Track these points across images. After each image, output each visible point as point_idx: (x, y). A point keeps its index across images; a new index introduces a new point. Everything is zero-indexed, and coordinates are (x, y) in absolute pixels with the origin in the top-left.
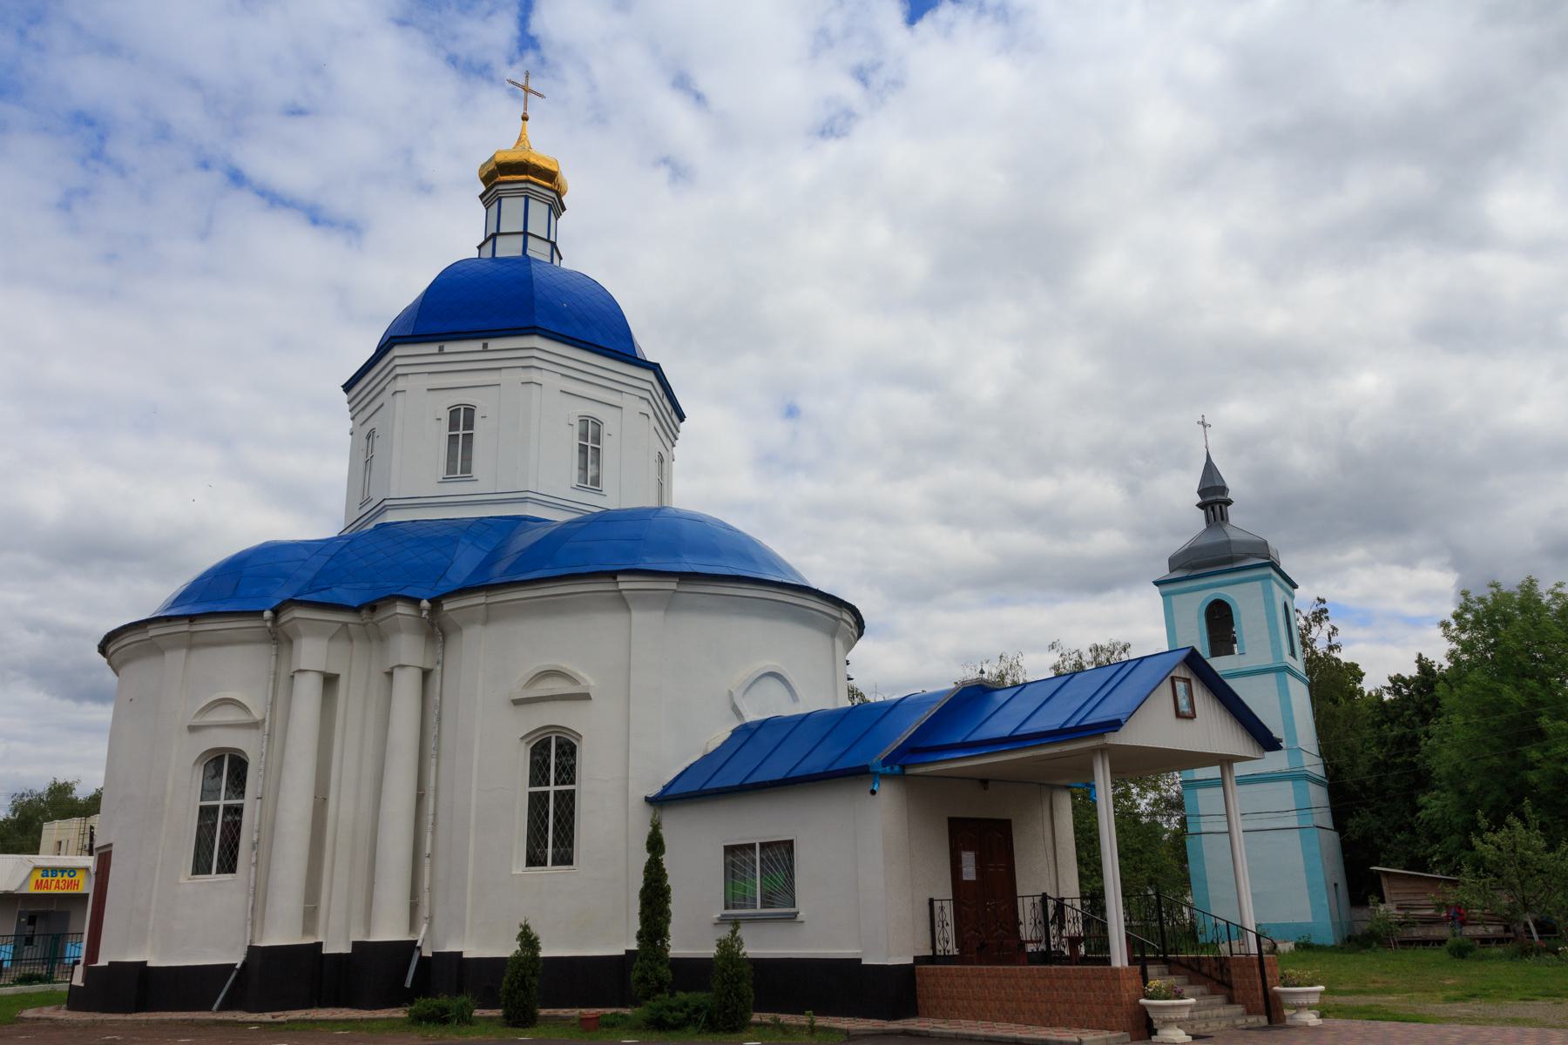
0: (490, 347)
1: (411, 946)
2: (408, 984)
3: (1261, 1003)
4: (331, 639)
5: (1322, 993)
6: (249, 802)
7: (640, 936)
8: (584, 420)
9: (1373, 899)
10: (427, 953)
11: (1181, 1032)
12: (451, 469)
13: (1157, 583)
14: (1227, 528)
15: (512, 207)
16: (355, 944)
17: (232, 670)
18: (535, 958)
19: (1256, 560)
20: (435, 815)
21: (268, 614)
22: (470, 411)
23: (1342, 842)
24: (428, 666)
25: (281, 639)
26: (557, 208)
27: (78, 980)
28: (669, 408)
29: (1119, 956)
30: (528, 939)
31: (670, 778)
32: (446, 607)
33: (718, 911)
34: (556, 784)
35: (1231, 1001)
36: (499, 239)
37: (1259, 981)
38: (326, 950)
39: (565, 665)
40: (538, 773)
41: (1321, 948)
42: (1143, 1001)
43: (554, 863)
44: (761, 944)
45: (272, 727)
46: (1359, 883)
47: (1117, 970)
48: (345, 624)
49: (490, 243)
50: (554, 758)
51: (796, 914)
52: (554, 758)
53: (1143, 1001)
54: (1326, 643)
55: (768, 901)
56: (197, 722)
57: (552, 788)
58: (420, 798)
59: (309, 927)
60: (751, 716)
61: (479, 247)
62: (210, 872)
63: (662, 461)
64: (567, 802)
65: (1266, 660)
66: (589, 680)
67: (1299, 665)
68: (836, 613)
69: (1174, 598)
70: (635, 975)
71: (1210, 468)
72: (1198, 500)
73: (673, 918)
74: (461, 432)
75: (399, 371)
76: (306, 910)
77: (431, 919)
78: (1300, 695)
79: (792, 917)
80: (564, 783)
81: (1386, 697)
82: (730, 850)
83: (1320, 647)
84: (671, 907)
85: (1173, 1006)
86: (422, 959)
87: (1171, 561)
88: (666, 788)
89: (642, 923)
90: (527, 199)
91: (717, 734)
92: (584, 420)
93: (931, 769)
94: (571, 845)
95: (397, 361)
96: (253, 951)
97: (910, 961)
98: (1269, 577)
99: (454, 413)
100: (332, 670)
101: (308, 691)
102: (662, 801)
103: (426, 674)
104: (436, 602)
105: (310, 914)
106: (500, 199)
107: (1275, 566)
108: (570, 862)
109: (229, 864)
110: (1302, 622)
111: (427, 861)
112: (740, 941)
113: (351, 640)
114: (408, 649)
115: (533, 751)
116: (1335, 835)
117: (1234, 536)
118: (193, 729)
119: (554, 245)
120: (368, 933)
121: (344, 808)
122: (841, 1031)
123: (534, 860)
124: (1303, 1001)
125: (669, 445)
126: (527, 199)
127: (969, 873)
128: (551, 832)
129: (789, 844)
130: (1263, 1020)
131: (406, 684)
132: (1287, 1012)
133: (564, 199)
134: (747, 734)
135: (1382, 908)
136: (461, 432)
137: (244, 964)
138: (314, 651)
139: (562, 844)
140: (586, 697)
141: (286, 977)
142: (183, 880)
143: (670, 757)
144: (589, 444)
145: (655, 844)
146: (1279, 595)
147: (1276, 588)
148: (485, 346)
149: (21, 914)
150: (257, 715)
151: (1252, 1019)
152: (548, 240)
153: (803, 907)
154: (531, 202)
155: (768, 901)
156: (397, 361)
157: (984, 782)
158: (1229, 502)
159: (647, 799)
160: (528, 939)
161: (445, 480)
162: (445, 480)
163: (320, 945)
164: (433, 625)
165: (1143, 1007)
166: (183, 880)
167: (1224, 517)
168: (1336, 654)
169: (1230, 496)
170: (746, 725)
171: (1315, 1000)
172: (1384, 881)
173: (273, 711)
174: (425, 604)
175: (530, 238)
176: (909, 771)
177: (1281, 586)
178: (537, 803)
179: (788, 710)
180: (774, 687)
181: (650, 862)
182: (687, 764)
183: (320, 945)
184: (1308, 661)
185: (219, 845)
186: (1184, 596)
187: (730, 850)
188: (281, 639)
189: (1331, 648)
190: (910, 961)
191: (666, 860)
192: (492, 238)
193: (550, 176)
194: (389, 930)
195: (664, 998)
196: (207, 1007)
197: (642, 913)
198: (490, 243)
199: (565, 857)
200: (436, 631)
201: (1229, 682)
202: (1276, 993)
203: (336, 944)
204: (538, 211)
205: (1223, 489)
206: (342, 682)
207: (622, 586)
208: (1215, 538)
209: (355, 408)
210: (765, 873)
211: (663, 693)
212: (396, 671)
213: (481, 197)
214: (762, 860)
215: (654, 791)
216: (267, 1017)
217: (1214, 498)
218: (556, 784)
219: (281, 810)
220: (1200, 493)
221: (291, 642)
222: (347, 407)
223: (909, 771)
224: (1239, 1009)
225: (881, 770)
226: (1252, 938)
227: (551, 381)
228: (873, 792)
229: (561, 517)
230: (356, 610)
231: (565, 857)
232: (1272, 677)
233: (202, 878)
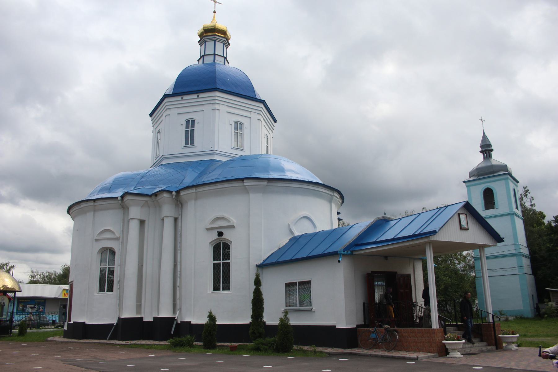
0: (184, 98)
1: (173, 319)
2: (172, 333)
3: (494, 341)
4: (142, 207)
7: (252, 317)
8: (236, 123)
9: (546, 300)
10: (179, 322)
11: (459, 353)
12: (186, 143)
13: (464, 182)
14: (492, 160)
15: (210, 45)
16: (154, 318)
17: (109, 220)
18: (215, 324)
19: (502, 172)
20: (181, 271)
22: (193, 121)
23: (535, 279)
24: (176, 217)
26: (227, 44)
27: (65, 328)
28: (270, 117)
29: (435, 323)
30: (212, 318)
31: (266, 257)
33: (283, 308)
34: (223, 260)
35: (482, 341)
36: (205, 57)
37: (493, 333)
38: (145, 319)
39: (225, 215)
40: (216, 257)
41: (527, 319)
42: (444, 342)
43: (223, 289)
44: (295, 321)
45: (123, 239)
46: (541, 293)
47: (434, 329)
48: (147, 201)
49: (202, 59)
50: (222, 250)
51: (312, 309)
52: (222, 250)
53: (444, 342)
54: (530, 204)
55: (301, 304)
56: (98, 238)
57: (221, 262)
58: (175, 266)
59: (139, 312)
60: (297, 233)
61: (198, 61)
63: (267, 138)
64: (227, 267)
65: (507, 211)
66: (234, 221)
67: (519, 212)
68: (332, 194)
69: (471, 187)
70: (250, 331)
71: (485, 137)
72: (480, 150)
73: (265, 310)
74: (190, 129)
75: (217, 102)
76: (137, 305)
77: (180, 309)
78: (520, 224)
80: (226, 260)
81: (553, 225)
82: (288, 285)
83: (528, 205)
84: (264, 306)
85: (456, 343)
86: (177, 324)
87: (470, 173)
88: (264, 261)
89: (253, 312)
90: (215, 41)
91: (284, 240)
92: (236, 123)
93: (363, 252)
94: (229, 283)
96: (119, 319)
97: (355, 327)
98: (508, 178)
99: (187, 122)
100: (143, 218)
101: (134, 226)
102: (261, 267)
103: (176, 220)
104: (178, 192)
105: (139, 307)
106: (205, 42)
107: (510, 174)
108: (229, 289)
109: (110, 289)
110: (520, 196)
111: (178, 288)
112: (288, 319)
113: (149, 207)
116: (533, 277)
117: (494, 163)
118: (97, 240)
119: (225, 58)
120: (158, 314)
121: (148, 269)
122: (327, 353)
124: (510, 340)
125: (270, 132)
126: (215, 41)
127: (378, 294)
128: (221, 279)
129: (309, 282)
130: (494, 348)
131: (168, 225)
132: (504, 345)
133: (229, 41)
134: (295, 240)
135: (550, 303)
136: (190, 129)
137: (117, 324)
139: (226, 283)
140: (233, 227)
142: (95, 294)
143: (265, 249)
144: (238, 132)
145: (258, 282)
146: (512, 185)
147: (510, 183)
148: (198, 96)
149: (61, 305)
150: (117, 235)
151: (489, 348)
152: (223, 56)
153: (314, 307)
154: (217, 42)
155: (301, 304)
156: (166, 104)
157: (386, 257)
158: (492, 150)
159: (257, 266)
160: (212, 318)
161: (184, 147)
162: (184, 147)
163: (142, 318)
164: (177, 201)
165: (444, 344)
166: (95, 294)
167: (490, 156)
168: (533, 208)
169: (492, 148)
171: (515, 340)
172: (551, 294)
173: (123, 233)
174: (174, 193)
175: (216, 56)
176: (354, 253)
177: (512, 182)
178: (216, 267)
179: (311, 231)
180: (306, 223)
181: (255, 289)
182: (272, 252)
183: (142, 318)
184: (523, 212)
185: (107, 282)
186: (474, 187)
187: (288, 285)
189: (532, 205)
190: (355, 327)
191: (263, 289)
192: (202, 57)
193: (224, 32)
194: (166, 313)
195: (261, 340)
196: (106, 339)
197: (253, 308)
198: (202, 59)
199: (227, 287)
201: (487, 220)
202: (500, 337)
203: (148, 318)
204: (219, 46)
205: (490, 145)
206: (146, 222)
207: (245, 184)
208: (488, 164)
209: (154, 123)
210: (300, 291)
212: (165, 219)
213: (199, 42)
214: (299, 289)
215: (259, 262)
216: (124, 343)
217: (486, 149)
218: (223, 260)
219: (127, 270)
220: (481, 147)
221: (128, 208)
222: (151, 122)
223: (354, 253)
224: (485, 343)
225: (342, 253)
226: (491, 316)
227: (223, 108)
229: (224, 159)
231: (227, 287)
232: (509, 217)
233: (102, 293)
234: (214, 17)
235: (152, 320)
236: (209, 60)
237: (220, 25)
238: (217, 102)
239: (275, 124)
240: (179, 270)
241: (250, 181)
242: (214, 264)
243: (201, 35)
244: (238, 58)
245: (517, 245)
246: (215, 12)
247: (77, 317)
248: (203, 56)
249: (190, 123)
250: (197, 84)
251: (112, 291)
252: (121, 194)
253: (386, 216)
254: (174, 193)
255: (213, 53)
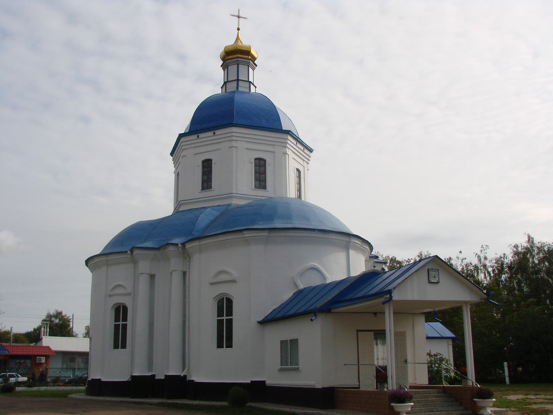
0: (200, 137)
5: (412, 406)
6: (129, 323)
20: (189, 328)
21: (129, 252)
25: (135, 262)
28: (302, 148)
32: (187, 247)
36: (228, 84)
40: (220, 313)
49: (224, 87)
50: (225, 306)
51: (298, 368)
52: (225, 306)
56: (111, 293)
58: (184, 322)
59: (150, 369)
60: (302, 287)
62: (118, 348)
75: (234, 138)
79: (297, 369)
80: (230, 316)
91: (288, 295)
95: (234, 134)
101: (143, 281)
103: (184, 273)
106: (228, 67)
109: (124, 346)
114: (176, 264)
115: (116, 310)
123: (220, 345)
128: (225, 336)
131: (177, 279)
134: (300, 294)
138: (144, 266)
140: (234, 281)
141: (140, 387)
150: (129, 290)
153: (300, 366)
154: (240, 66)
157: (375, 314)
159: (258, 322)
170: (299, 290)
174: (180, 245)
178: (117, 327)
183: (154, 376)
188: (135, 262)
198: (224, 87)
200: (186, 255)
203: (160, 376)
207: (245, 235)
209: (176, 162)
211: (261, 278)
212: (173, 273)
213: (221, 66)
215: (261, 319)
228: (312, 320)
229: (242, 202)
230: (158, 249)
234: (238, 36)
235: (163, 378)
236: (232, 87)
237: (245, 42)
238: (234, 138)
239: (311, 155)
240: (187, 326)
241: (250, 232)
242: (218, 320)
243: (224, 59)
244: (264, 81)
245: (466, 307)
246: (238, 29)
247: (94, 375)
248: (228, 82)
249: (207, 165)
250: (213, 117)
251: (232, 347)
252: (130, 248)
253: (376, 269)
254: (180, 245)
255: (236, 78)
